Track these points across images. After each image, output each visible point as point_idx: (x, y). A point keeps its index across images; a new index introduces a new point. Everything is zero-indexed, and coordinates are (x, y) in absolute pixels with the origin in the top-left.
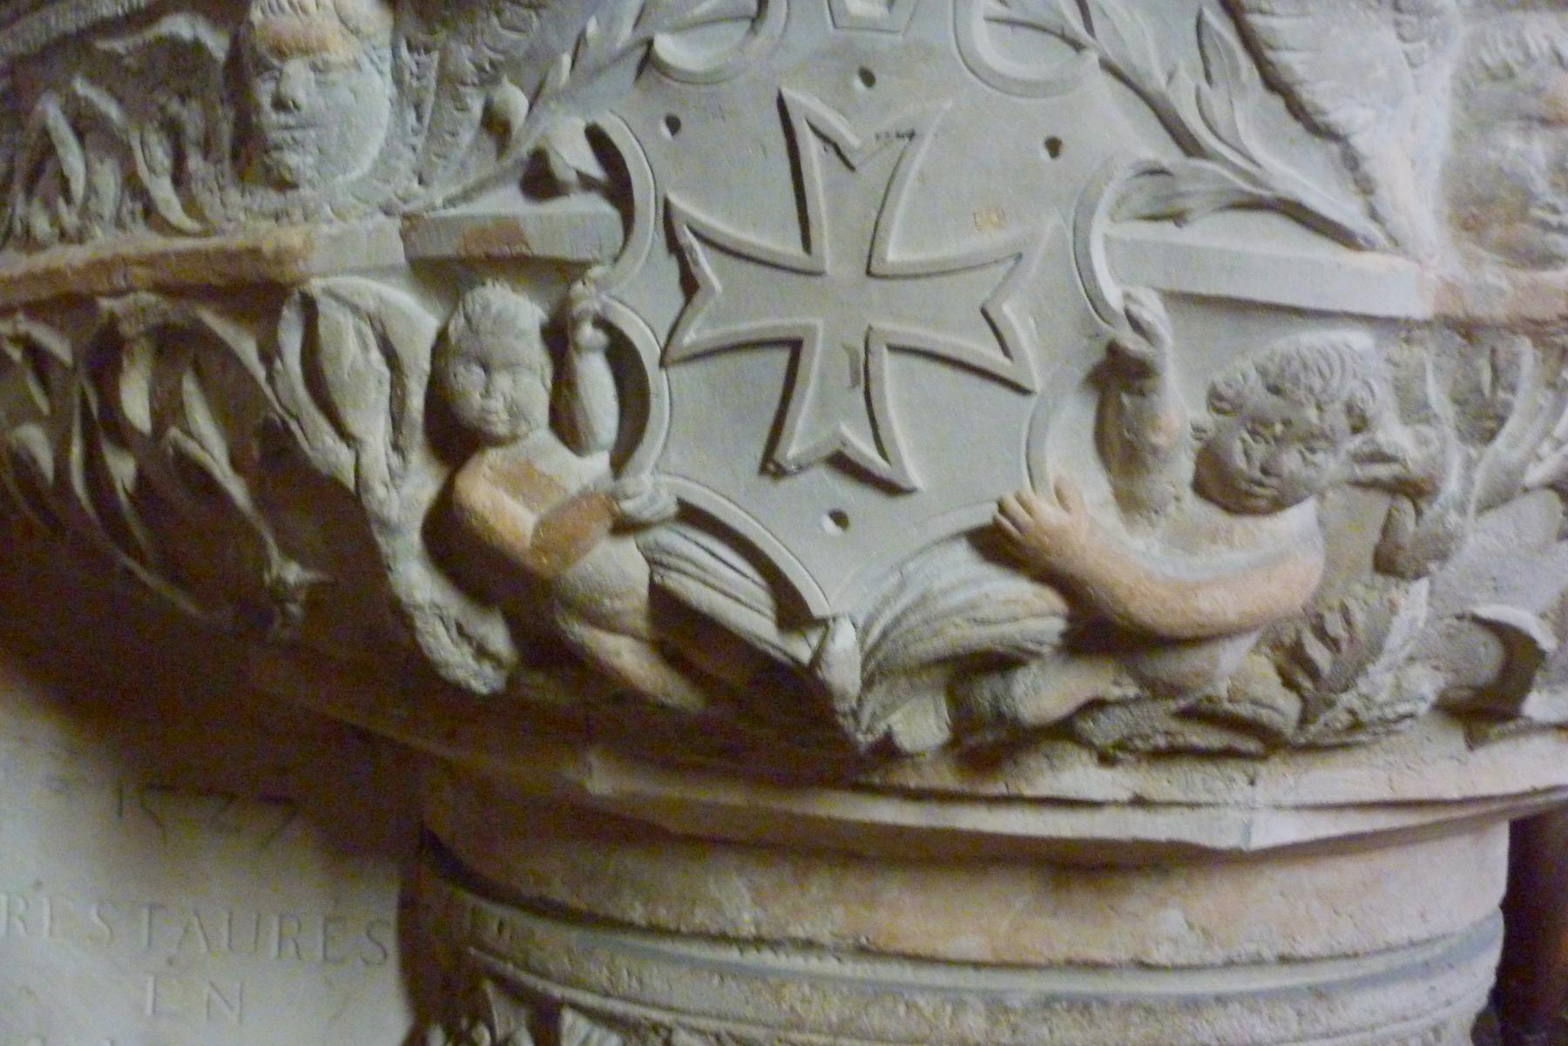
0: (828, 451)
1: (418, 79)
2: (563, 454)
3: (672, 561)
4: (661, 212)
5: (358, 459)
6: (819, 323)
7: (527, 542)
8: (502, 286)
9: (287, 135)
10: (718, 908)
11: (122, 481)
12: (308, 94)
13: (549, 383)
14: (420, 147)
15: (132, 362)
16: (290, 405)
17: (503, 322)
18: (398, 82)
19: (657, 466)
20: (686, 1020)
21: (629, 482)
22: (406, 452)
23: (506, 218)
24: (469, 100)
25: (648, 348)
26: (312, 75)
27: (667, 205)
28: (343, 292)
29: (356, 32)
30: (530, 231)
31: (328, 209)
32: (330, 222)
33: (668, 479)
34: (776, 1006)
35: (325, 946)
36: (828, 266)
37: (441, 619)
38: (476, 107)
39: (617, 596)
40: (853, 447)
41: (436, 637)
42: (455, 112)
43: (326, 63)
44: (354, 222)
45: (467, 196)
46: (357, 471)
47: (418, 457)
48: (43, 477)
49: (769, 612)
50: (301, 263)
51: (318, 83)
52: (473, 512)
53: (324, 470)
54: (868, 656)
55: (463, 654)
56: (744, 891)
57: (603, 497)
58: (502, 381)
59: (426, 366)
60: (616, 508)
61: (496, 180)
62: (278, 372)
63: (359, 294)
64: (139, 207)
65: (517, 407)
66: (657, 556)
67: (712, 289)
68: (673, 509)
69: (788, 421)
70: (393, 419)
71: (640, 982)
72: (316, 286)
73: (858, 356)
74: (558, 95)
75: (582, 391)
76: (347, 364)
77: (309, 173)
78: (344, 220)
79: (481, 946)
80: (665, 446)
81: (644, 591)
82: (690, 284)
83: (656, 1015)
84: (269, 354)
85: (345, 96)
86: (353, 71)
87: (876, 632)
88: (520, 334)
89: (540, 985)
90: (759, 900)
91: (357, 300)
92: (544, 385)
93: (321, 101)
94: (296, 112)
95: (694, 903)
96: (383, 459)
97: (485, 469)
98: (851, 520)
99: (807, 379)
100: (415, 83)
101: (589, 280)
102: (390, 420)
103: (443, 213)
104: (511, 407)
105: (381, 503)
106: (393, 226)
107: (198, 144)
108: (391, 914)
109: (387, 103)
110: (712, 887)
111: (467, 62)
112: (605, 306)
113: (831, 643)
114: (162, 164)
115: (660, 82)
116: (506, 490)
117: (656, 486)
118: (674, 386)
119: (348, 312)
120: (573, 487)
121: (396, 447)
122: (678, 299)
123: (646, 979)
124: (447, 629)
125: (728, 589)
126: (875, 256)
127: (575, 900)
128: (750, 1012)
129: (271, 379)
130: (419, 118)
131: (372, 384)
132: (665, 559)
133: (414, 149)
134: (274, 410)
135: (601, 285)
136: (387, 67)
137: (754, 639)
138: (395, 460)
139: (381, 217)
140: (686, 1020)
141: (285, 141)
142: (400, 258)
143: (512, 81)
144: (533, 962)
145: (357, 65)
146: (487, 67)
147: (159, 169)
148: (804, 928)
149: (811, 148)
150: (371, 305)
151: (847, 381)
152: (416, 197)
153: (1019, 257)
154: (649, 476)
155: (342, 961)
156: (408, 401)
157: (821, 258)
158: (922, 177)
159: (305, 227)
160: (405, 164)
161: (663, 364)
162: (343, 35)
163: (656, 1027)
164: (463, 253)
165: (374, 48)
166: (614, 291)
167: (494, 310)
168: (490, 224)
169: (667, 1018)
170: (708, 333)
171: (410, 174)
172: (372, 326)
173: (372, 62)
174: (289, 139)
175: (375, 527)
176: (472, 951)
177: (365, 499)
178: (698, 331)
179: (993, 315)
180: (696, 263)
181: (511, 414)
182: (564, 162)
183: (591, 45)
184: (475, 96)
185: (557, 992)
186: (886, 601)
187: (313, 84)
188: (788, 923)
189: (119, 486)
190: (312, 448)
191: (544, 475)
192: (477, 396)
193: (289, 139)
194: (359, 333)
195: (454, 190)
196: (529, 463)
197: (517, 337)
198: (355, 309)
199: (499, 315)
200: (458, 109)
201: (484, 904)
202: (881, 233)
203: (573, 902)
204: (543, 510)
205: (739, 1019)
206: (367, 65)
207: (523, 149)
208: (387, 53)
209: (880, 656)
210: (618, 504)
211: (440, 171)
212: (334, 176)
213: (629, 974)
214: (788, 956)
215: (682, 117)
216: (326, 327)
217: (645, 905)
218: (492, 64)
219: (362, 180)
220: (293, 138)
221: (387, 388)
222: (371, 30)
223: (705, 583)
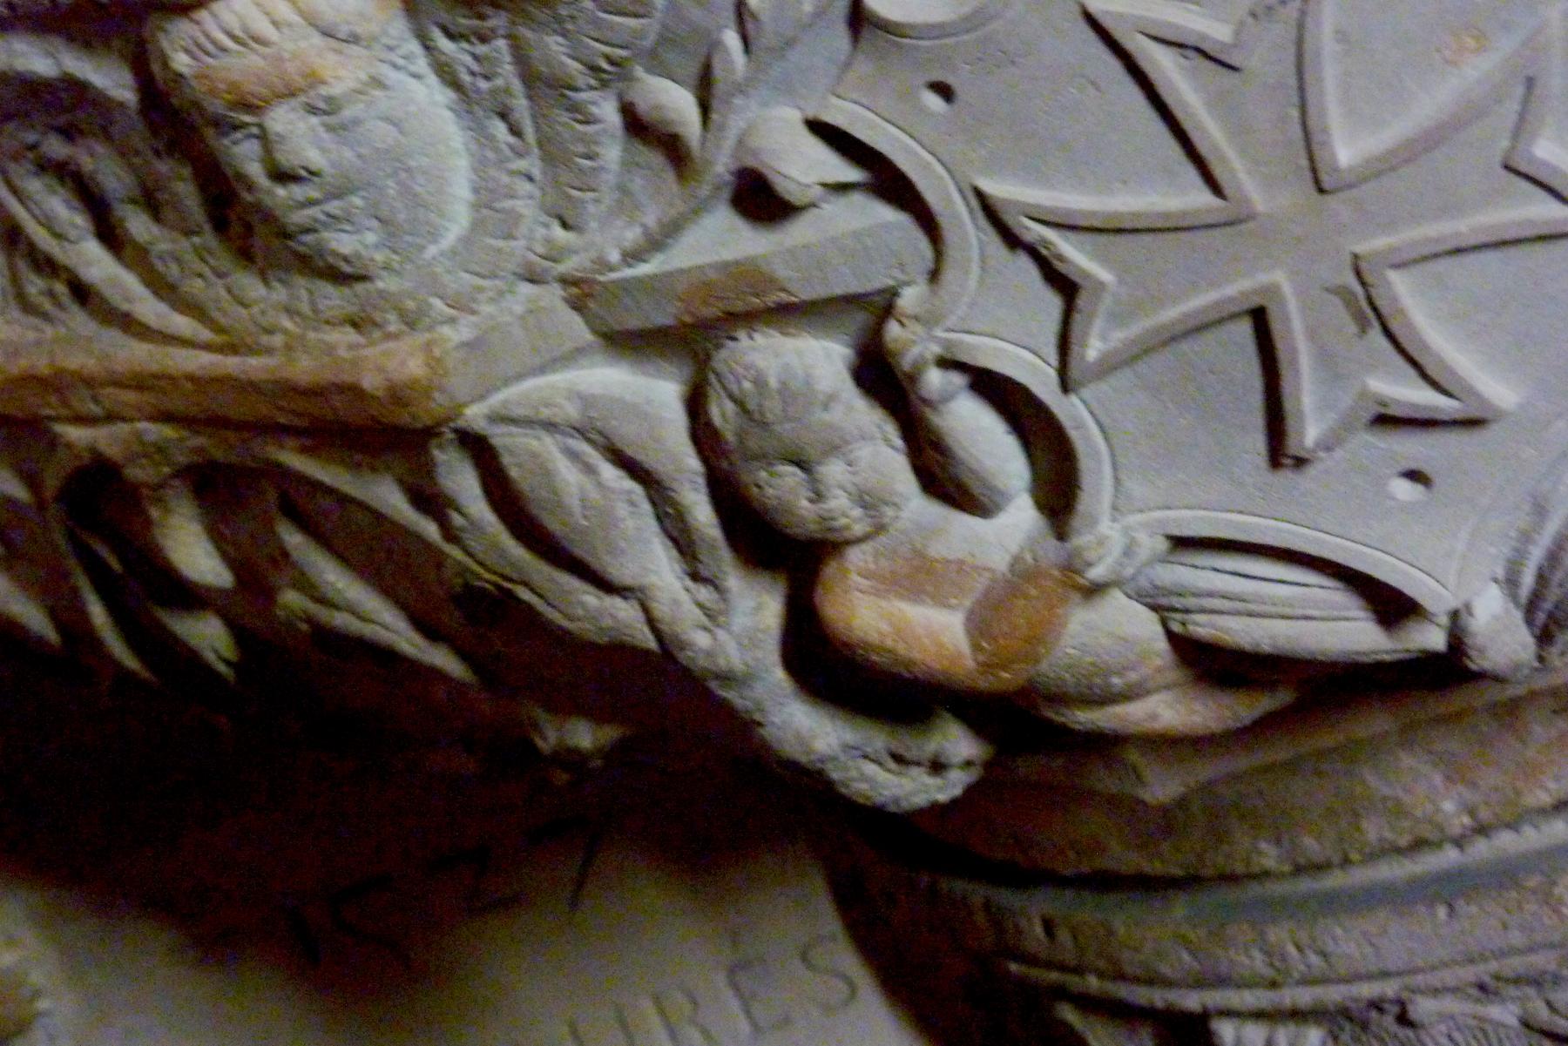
0: (1367, 415)
1: (487, 78)
2: (963, 523)
3: (1191, 602)
4: (974, 203)
5: (646, 610)
6: (1280, 277)
7: (970, 663)
8: (763, 333)
9: (314, 212)
10: (1398, 811)
11: (216, 651)
12: (323, 150)
13: (899, 443)
14: (536, 172)
15: (167, 511)
16: (507, 571)
17: (795, 395)
18: (454, 84)
19: (1115, 508)
20: (1420, 979)
21: (1081, 539)
22: (717, 582)
23: (737, 263)
24: (594, 110)
25: (1037, 376)
26: (314, 120)
27: (979, 194)
28: (519, 412)
29: (354, 39)
30: (782, 272)
31: (437, 303)
32: (452, 321)
33: (1139, 517)
34: (1554, 917)
35: (748, 1013)
36: (1259, 200)
37: (865, 757)
38: (608, 111)
39: (1124, 668)
40: (1398, 402)
41: (864, 778)
42: (578, 126)
43: (329, 99)
44: (487, 309)
45: (655, 243)
46: (651, 621)
47: (735, 579)
48: (41, 641)
49: (1362, 614)
50: (436, 395)
51: (330, 128)
52: (867, 646)
53: (603, 640)
54: (1530, 609)
55: (914, 780)
56: (1425, 769)
57: (1056, 573)
58: (833, 471)
59: (693, 463)
60: (1082, 581)
61: (698, 210)
62: (462, 529)
63: (547, 405)
64: (61, 288)
65: (868, 494)
66: (1164, 601)
67: (1101, 286)
68: (1162, 545)
69: (1288, 405)
70: (674, 541)
71: (1324, 955)
72: (475, 416)
73: (1353, 294)
74: (741, 89)
75: (961, 453)
76: (574, 504)
77: (379, 257)
78: (473, 312)
79: (1031, 960)
80: (1117, 481)
81: (1162, 644)
82: (1064, 285)
83: (1367, 990)
84: (431, 501)
85: (382, 134)
86: (377, 93)
87: (1528, 580)
88: (829, 401)
89: (1157, 997)
90: (1456, 773)
91: (545, 413)
92: (893, 447)
93: (348, 154)
94: (316, 179)
95: (1356, 815)
96: (684, 597)
97: (856, 578)
98: (1437, 480)
99: (1294, 351)
100: (483, 85)
101: (908, 317)
102: (670, 544)
103: (628, 272)
104: (861, 497)
105: (709, 654)
106: (553, 296)
107: (133, 201)
108: (829, 922)
109: (448, 114)
110: (1372, 779)
111: (569, 61)
112: (948, 344)
113: (1470, 618)
114: (76, 226)
115: (899, 46)
116: (902, 597)
117: (1126, 530)
118: (1094, 405)
119: (543, 434)
120: (1000, 562)
121: (695, 577)
122: (1052, 303)
123: (1330, 947)
124: (880, 764)
125: (1288, 611)
126: (1320, 166)
127: (1158, 864)
128: (1516, 938)
129: (450, 534)
130: (515, 131)
131: (622, 510)
132: (1176, 602)
133: (530, 179)
134: (479, 578)
135: (928, 320)
136: (422, 64)
137: (1354, 656)
138: (704, 593)
139: (526, 289)
140: (1420, 979)
141: (316, 220)
142: (589, 337)
143: (650, 70)
144: (1128, 969)
145: (377, 82)
146: (605, 66)
147: (72, 234)
148: (1547, 790)
149: (1163, 64)
150: (572, 412)
151: (1352, 328)
152: (567, 251)
153: (1530, 83)
154: (1110, 524)
155: (786, 1021)
156: (689, 519)
157: (1247, 201)
158: (1342, 36)
159: (421, 338)
160: (526, 204)
161: (1066, 386)
162: (335, 51)
163: (1377, 1005)
164: (688, 319)
165: (390, 49)
166: (952, 321)
167: (773, 382)
168: (713, 275)
169: (1389, 989)
170: (1119, 336)
171: (544, 218)
172: (589, 440)
173: (395, 66)
174: (323, 217)
175: (713, 685)
176: (1013, 967)
177: (683, 657)
178: (1104, 338)
179: (1523, 168)
180: (1061, 258)
181: (865, 506)
182: (799, 183)
183: (765, 17)
184: (601, 100)
185: (1192, 1001)
186: (1526, 538)
187: (321, 130)
188: (1518, 793)
189: (211, 657)
190: (571, 619)
191: (948, 561)
192: (805, 503)
193: (323, 217)
194: (573, 456)
195: (632, 236)
196: (919, 554)
197: (826, 407)
198: (550, 426)
199: (784, 389)
200: (581, 122)
201: (1007, 898)
202: (1317, 138)
203: (1156, 867)
204: (968, 603)
205: (1502, 954)
206: (392, 76)
207: (722, 165)
208: (414, 46)
209: (1548, 605)
210: (1083, 577)
211: (591, 208)
212: (422, 248)
213: (1299, 948)
214: (1536, 827)
215: (950, 80)
216: (519, 466)
217: (1278, 841)
218: (611, 61)
219: (467, 241)
220: (328, 215)
221: (646, 507)
222: (374, 28)
223: (1250, 614)
